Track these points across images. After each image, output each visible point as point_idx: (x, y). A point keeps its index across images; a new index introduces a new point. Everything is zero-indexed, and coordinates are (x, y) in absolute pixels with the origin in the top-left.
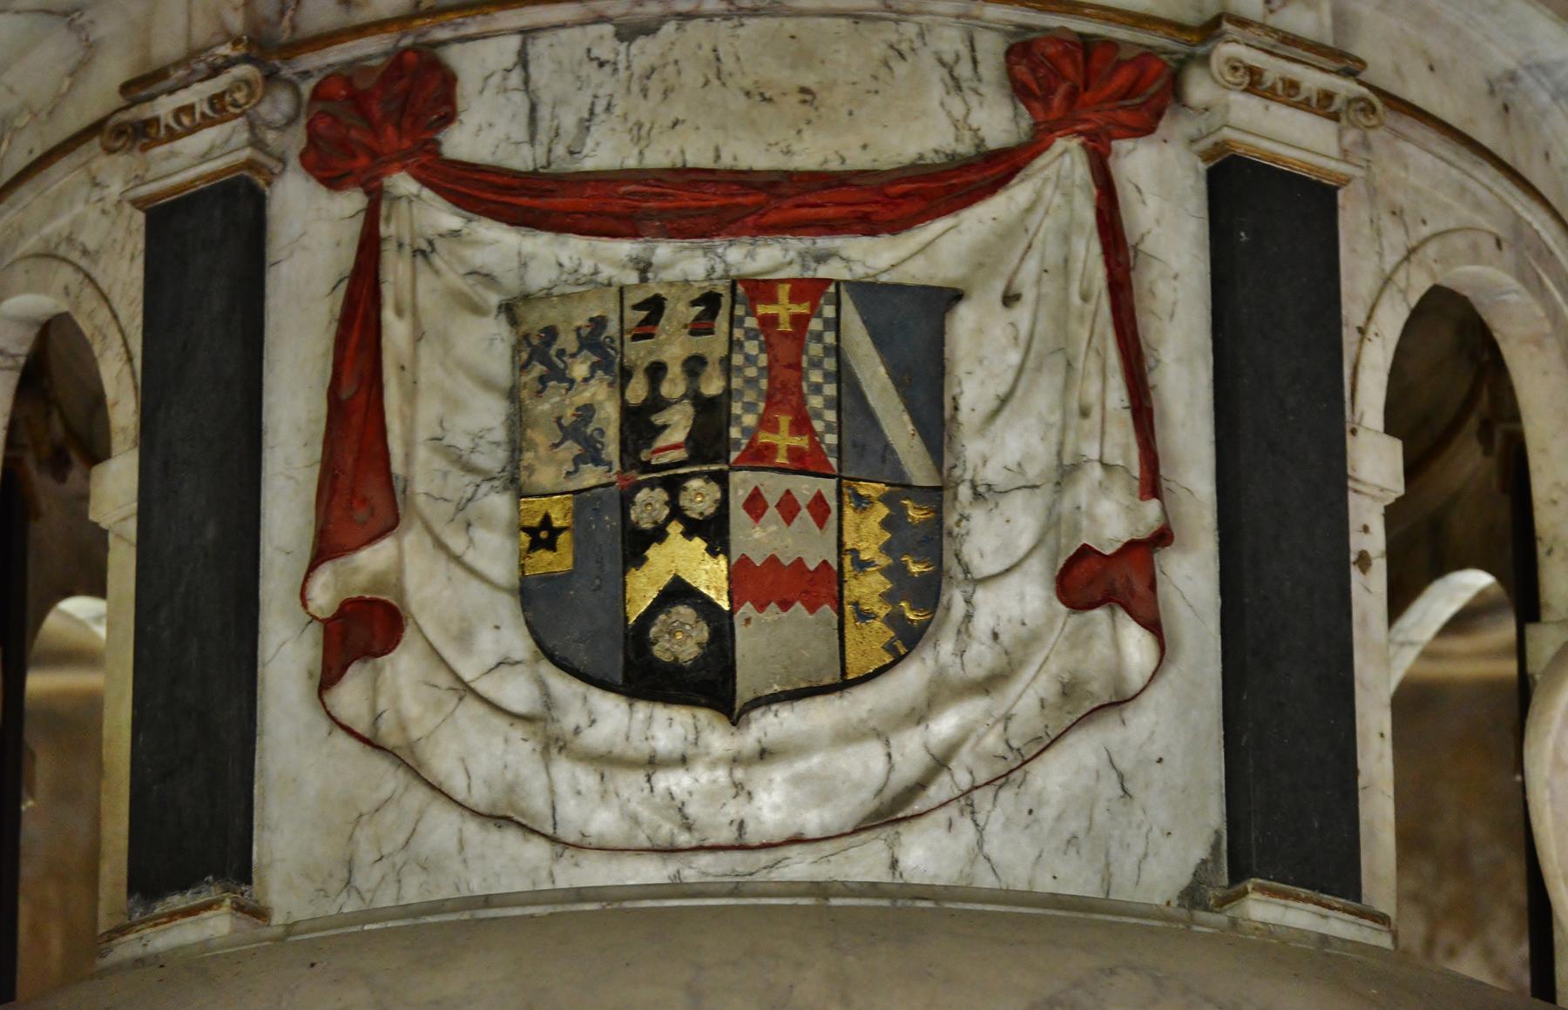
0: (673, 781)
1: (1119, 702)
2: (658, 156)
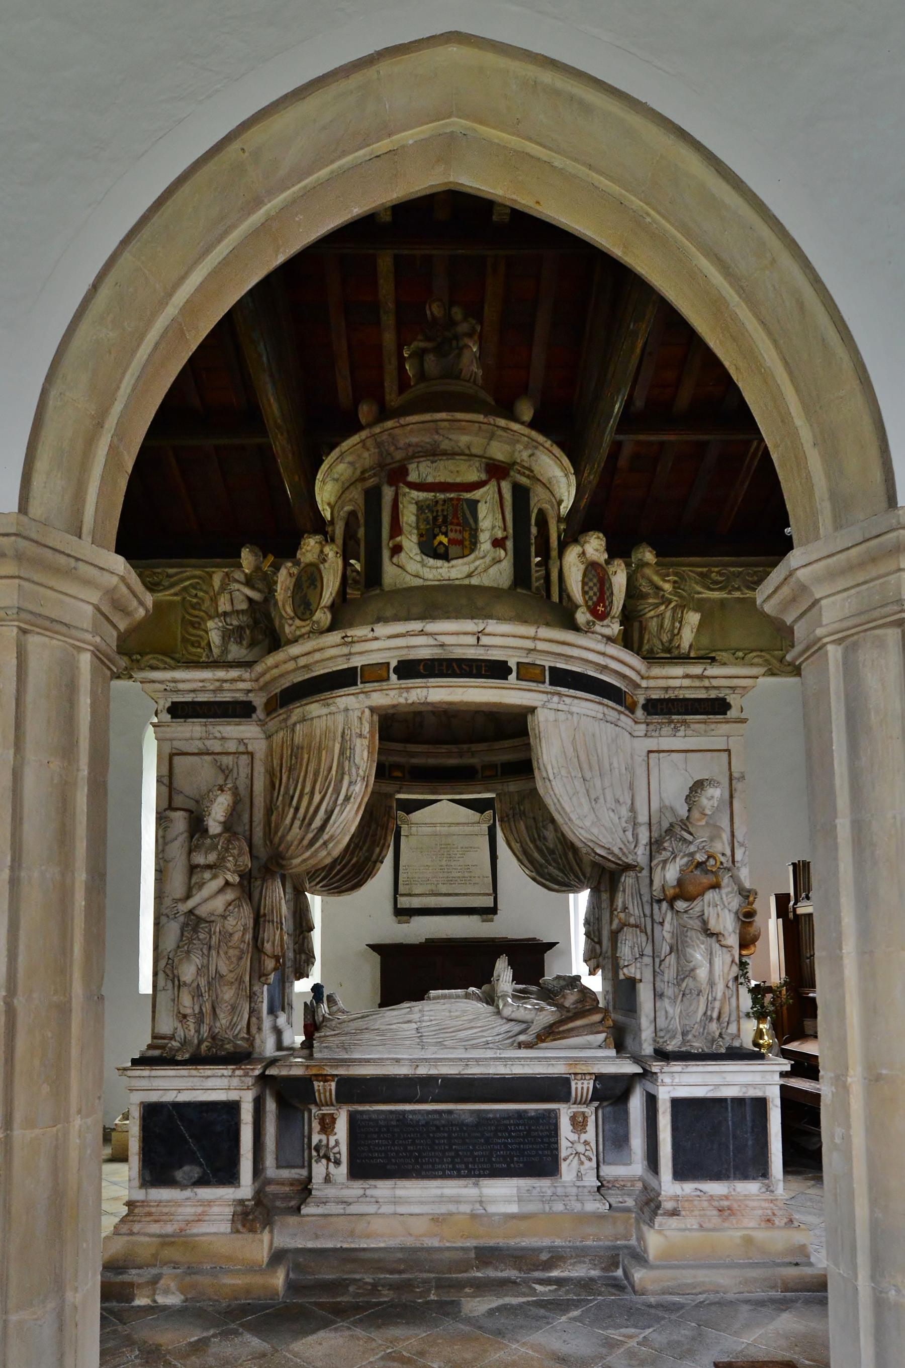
0: (440, 570)
1: (500, 561)
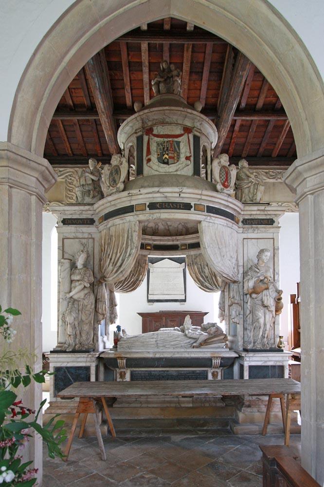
2: (165, 133)
